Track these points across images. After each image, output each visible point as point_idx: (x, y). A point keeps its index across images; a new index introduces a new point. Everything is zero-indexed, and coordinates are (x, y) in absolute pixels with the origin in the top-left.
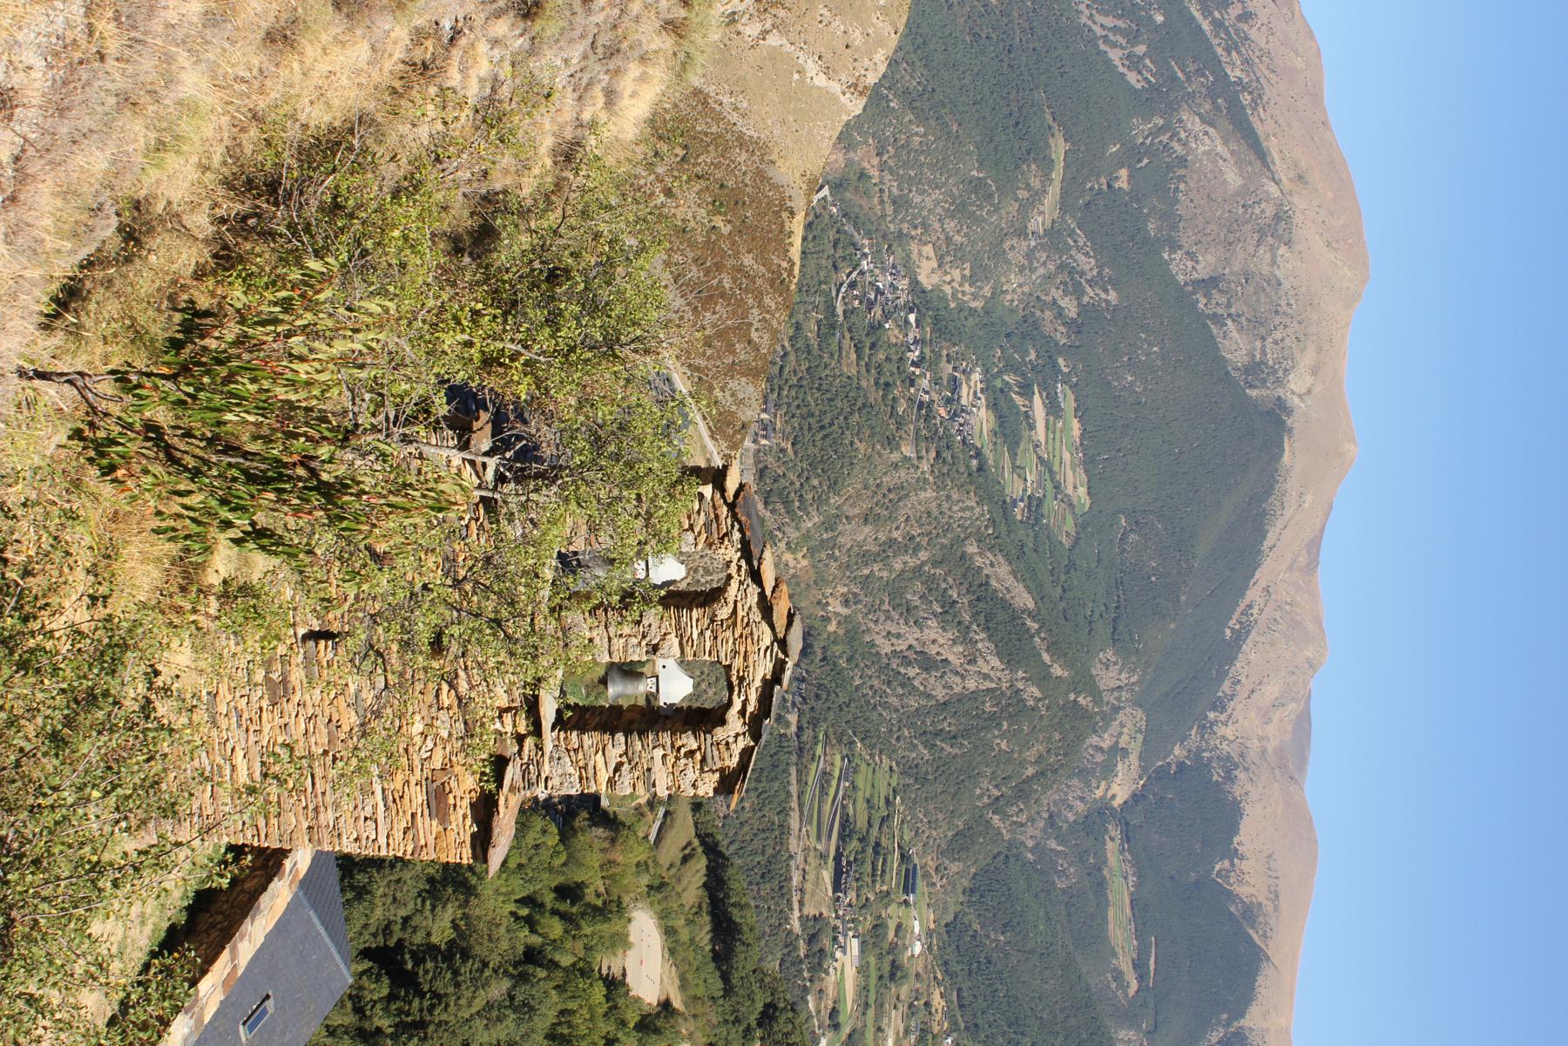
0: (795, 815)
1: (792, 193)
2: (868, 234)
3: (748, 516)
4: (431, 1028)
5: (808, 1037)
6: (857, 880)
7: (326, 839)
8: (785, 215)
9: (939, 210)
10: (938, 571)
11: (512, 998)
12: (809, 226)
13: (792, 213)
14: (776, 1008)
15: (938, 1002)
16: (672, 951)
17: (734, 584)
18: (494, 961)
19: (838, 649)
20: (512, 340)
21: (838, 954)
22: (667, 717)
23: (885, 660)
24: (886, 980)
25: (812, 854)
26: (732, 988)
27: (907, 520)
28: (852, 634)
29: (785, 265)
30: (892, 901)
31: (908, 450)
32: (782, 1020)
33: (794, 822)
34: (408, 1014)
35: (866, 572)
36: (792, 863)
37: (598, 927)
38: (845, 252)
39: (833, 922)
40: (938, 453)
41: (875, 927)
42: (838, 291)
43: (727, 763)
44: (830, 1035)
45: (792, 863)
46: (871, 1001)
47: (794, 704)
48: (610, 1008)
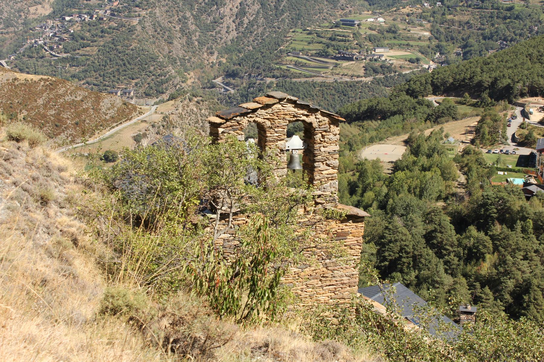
0: (316, 79)
1: (5, 79)
2: (25, 40)
3: (230, 113)
4: (416, 253)
5: (423, 74)
6: (347, 49)
7: (354, 280)
8: (16, 83)
9: (11, 3)
10: (196, 7)
11: (402, 215)
12: (21, 71)
13: (16, 79)
14: (408, 89)
15: (407, 10)
16: (381, 139)
17: (257, 119)
18: (385, 223)
19: (234, 57)
20: (178, 205)
21: (383, 59)
22: (308, 146)
23: (240, 34)
24: (396, 35)
25: (335, 71)
26: (398, 110)
27: (171, 23)
28: (227, 50)
29: (42, 83)
30: (358, 32)
31: (135, 22)
32: (414, 87)
33: (319, 80)
34: (409, 264)
35: (196, 43)
36: (339, 81)
37: (369, 175)
38: (34, 52)
39: (368, 61)
40: (137, 6)
41: (370, 41)
42: (55, 56)
43: (327, 122)
44: (422, 63)
45: (339, 81)
46: (406, 43)
47: (262, 80)
48: (408, 169)
